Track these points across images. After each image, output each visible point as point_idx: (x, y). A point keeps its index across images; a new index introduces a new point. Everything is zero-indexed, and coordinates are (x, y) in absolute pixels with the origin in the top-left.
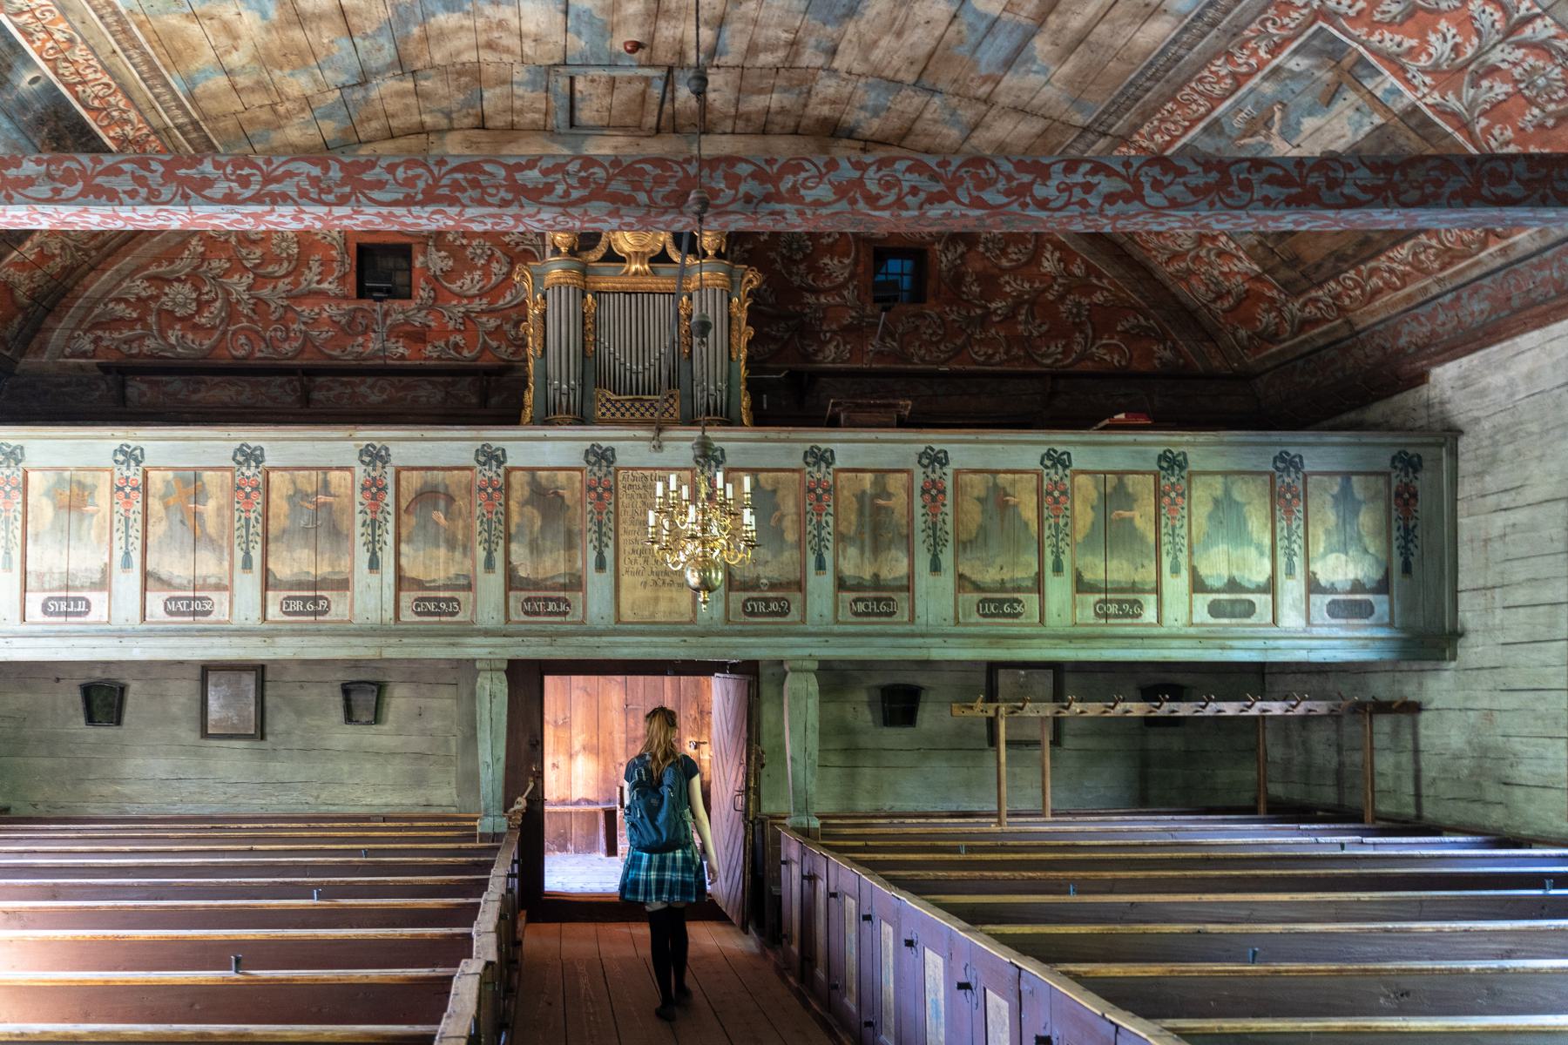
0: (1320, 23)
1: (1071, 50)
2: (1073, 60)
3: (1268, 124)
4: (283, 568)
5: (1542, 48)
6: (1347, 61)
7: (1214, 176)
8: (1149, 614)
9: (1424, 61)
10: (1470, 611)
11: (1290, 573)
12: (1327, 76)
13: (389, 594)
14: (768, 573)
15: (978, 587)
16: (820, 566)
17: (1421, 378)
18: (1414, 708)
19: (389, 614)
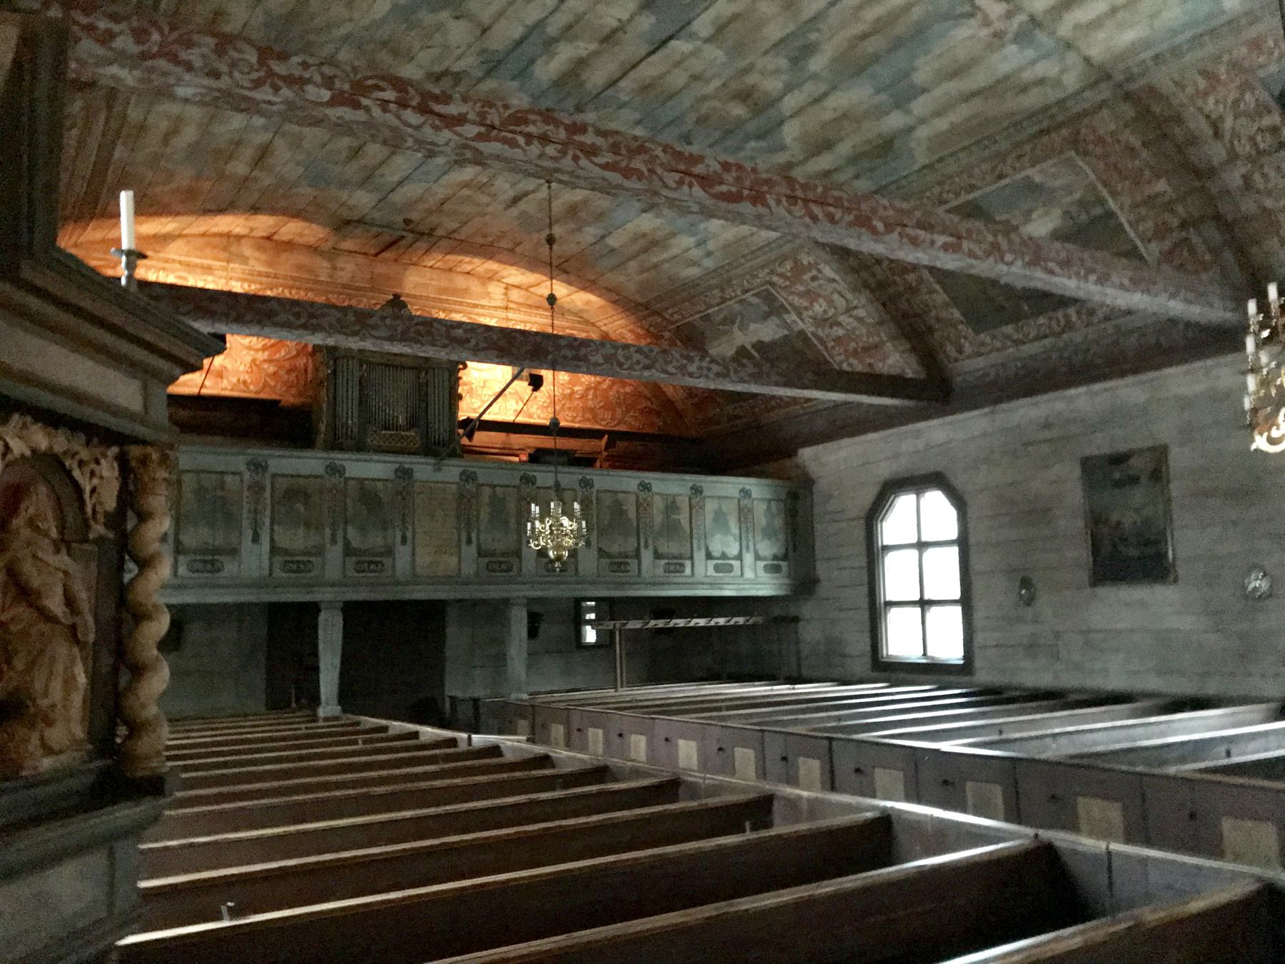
0: (768, 286)
1: (648, 270)
2: (646, 275)
3: (733, 322)
4: (189, 539)
5: (860, 320)
6: (777, 305)
7: (756, 370)
8: (688, 571)
9: (810, 313)
10: (821, 569)
11: (646, 547)
12: (766, 309)
13: (266, 556)
14: (499, 547)
15: (609, 556)
16: (469, 541)
17: (791, 453)
18: (796, 619)
19: (266, 572)
